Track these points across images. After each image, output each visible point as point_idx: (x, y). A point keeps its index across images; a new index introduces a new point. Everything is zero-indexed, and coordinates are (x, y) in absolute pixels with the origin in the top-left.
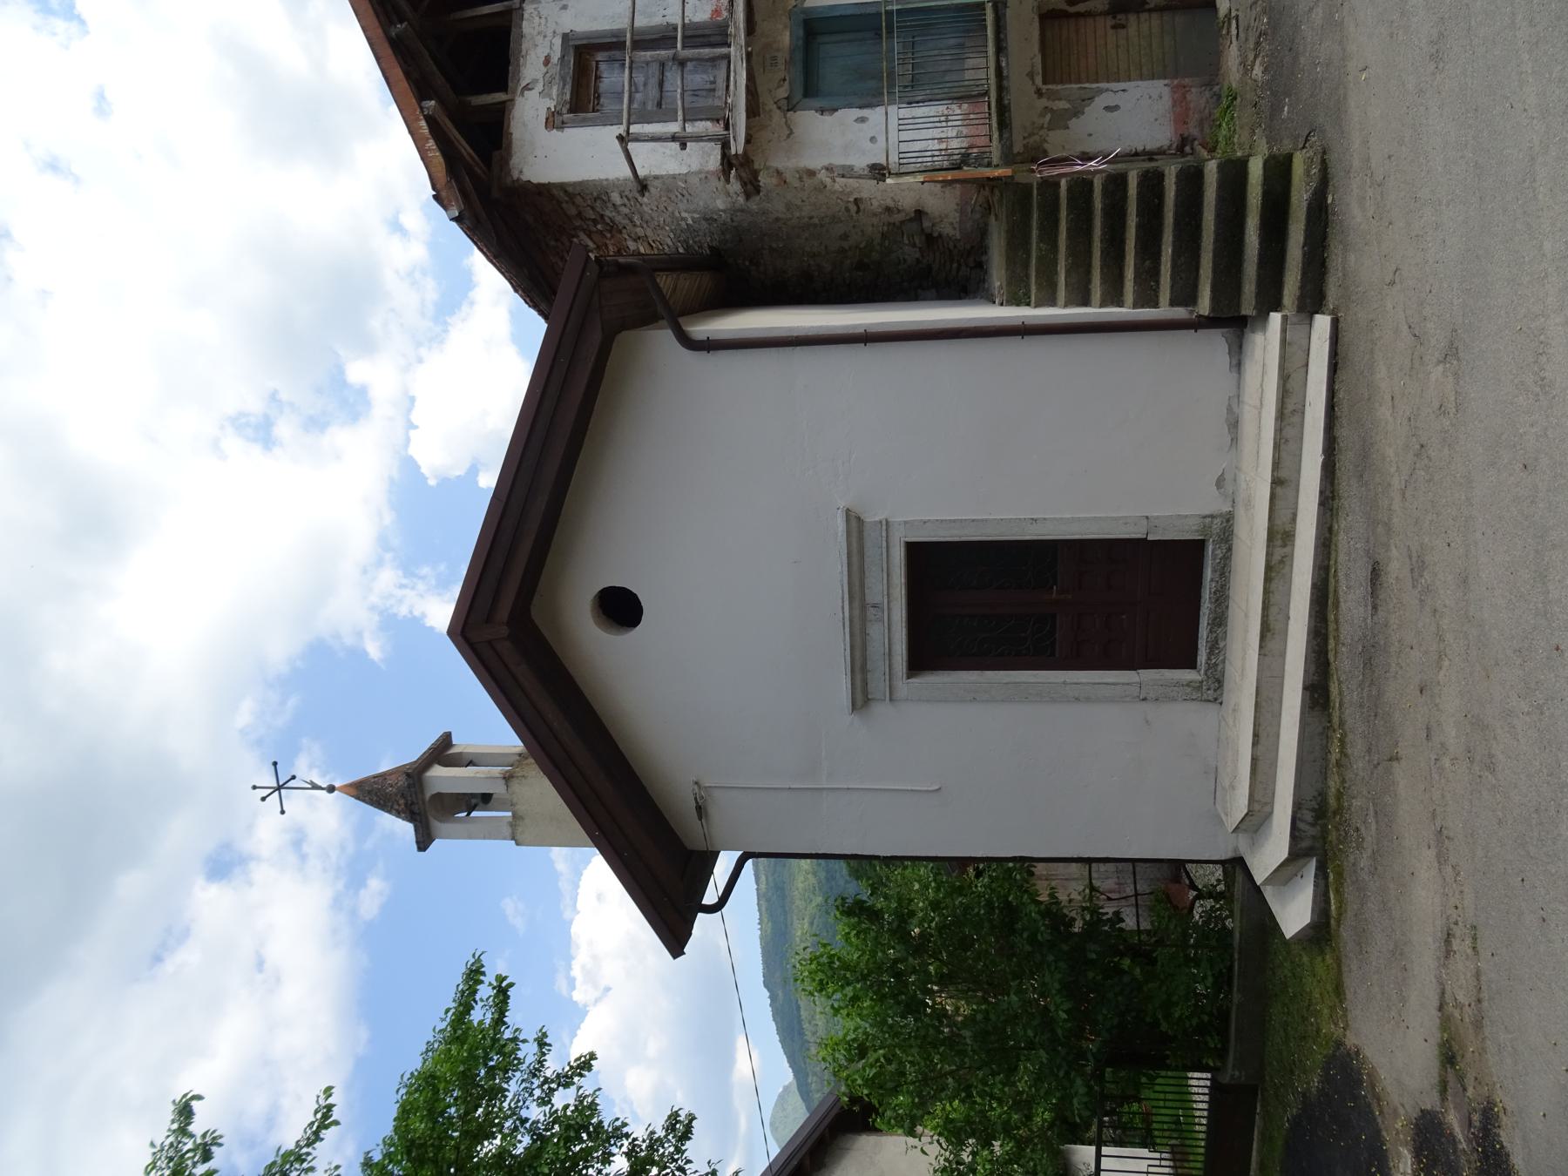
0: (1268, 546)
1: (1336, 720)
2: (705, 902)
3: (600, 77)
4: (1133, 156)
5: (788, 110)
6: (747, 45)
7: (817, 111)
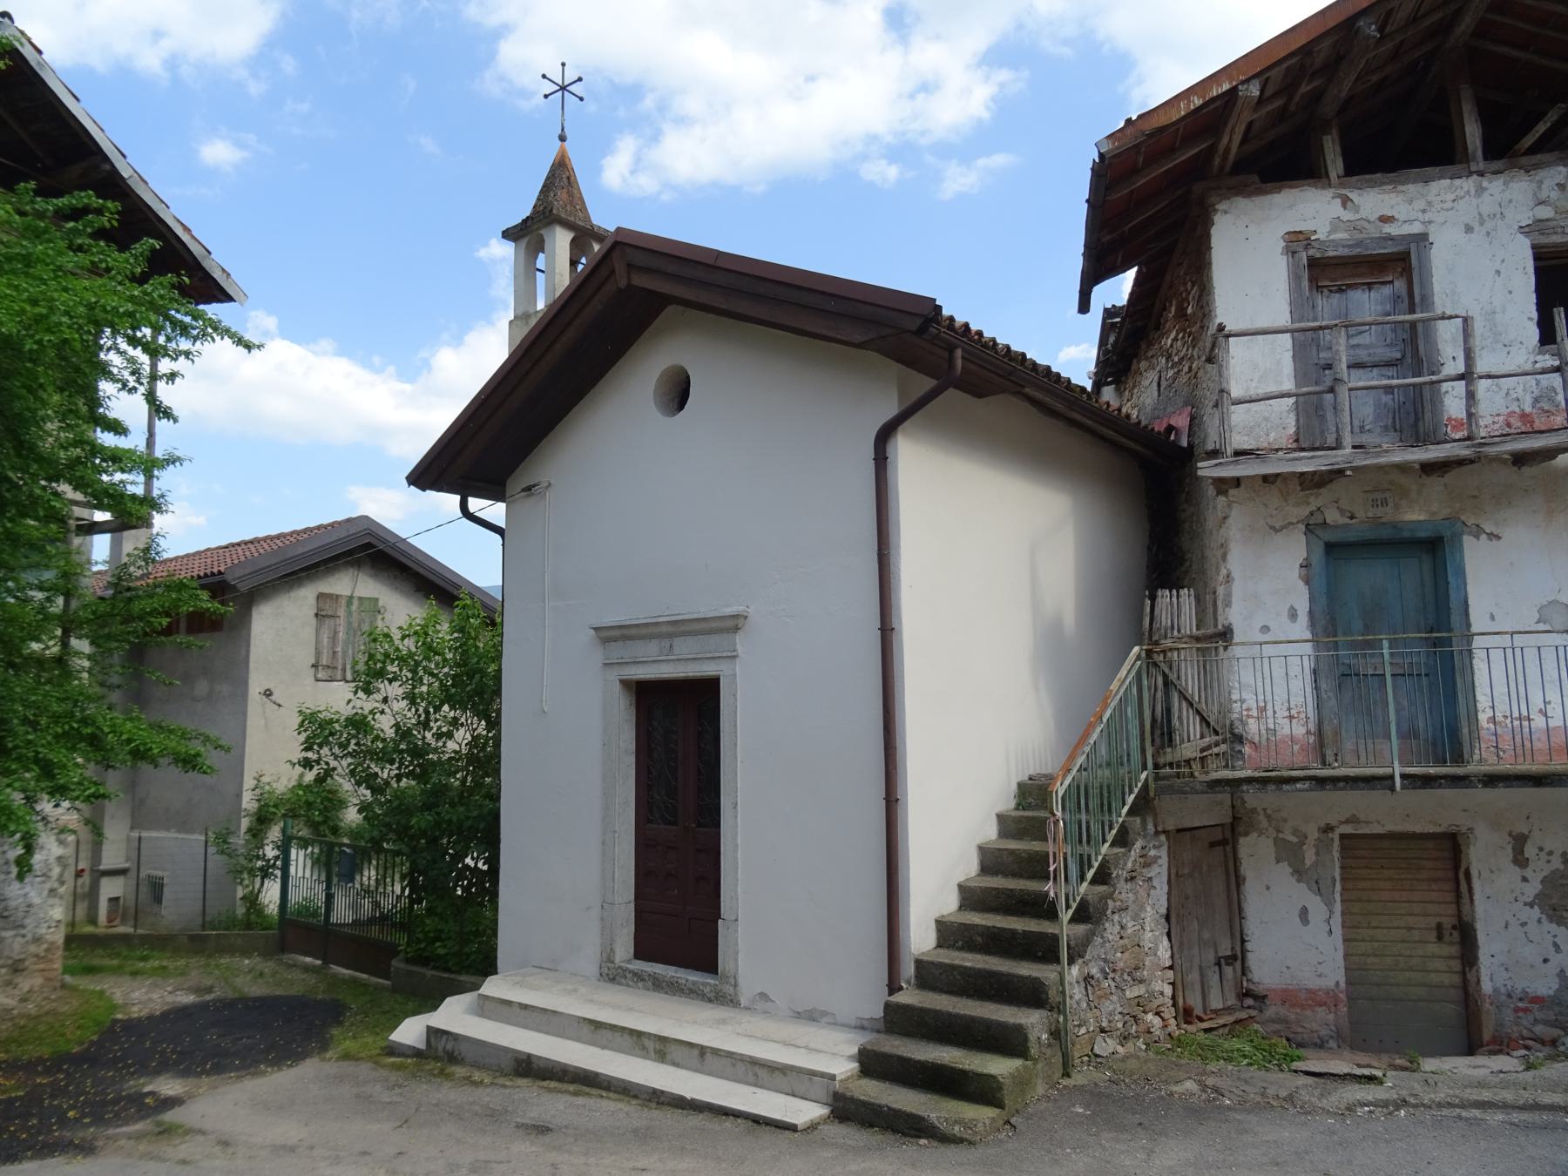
0: (655, 1035)
1: (501, 1081)
2: (470, 499)
3: (1370, 290)
4: (1242, 937)
5: (1307, 525)
6: (1354, 469)
7: (1306, 559)
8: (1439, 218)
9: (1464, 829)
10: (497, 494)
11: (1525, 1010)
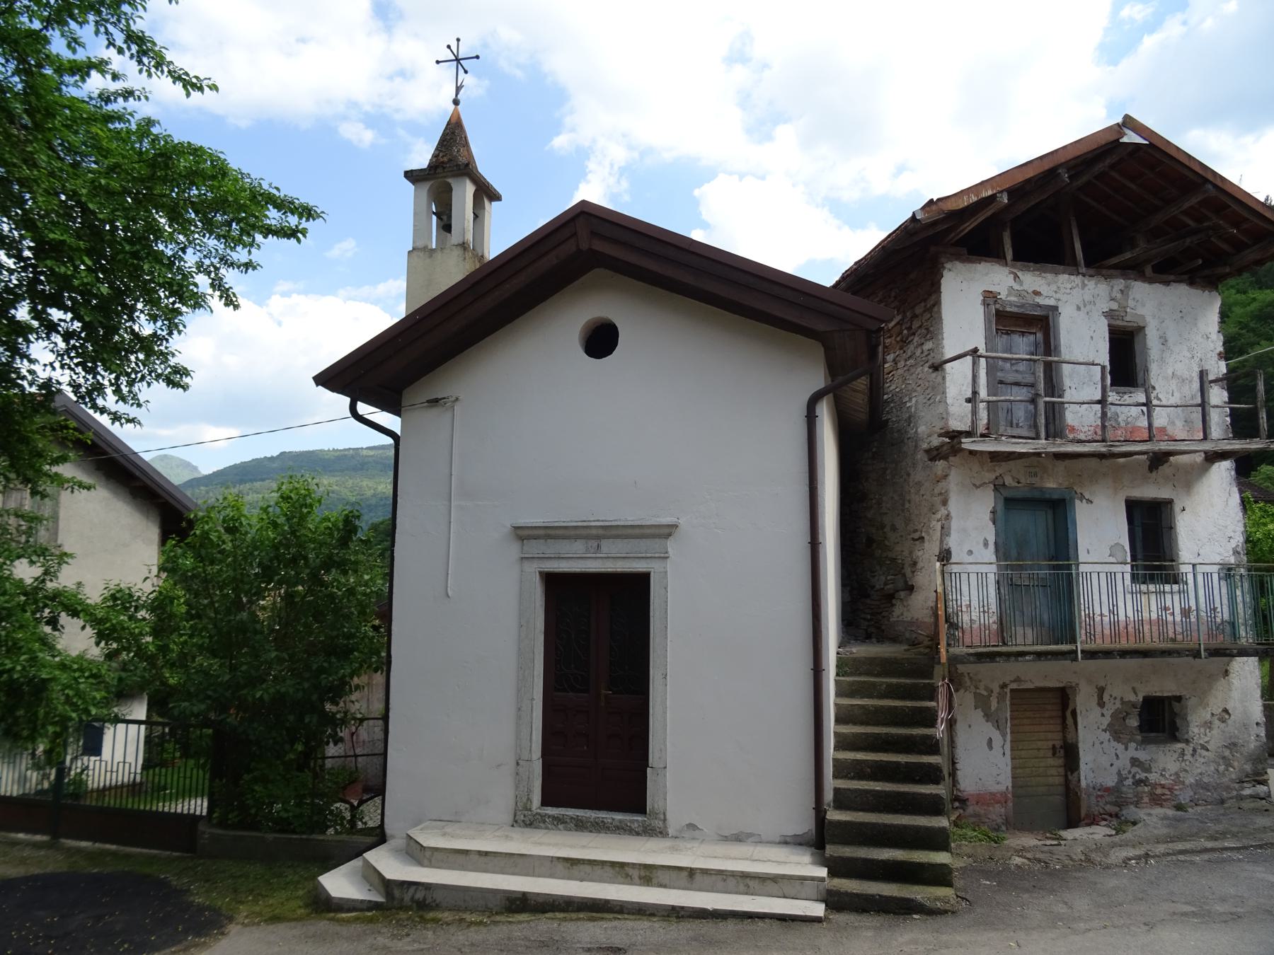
0: (640, 865)
1: (498, 918)
5: (995, 485)
7: (994, 508)
8: (1064, 298)
9: (1074, 685)
10: (393, 407)
11: (1101, 796)
